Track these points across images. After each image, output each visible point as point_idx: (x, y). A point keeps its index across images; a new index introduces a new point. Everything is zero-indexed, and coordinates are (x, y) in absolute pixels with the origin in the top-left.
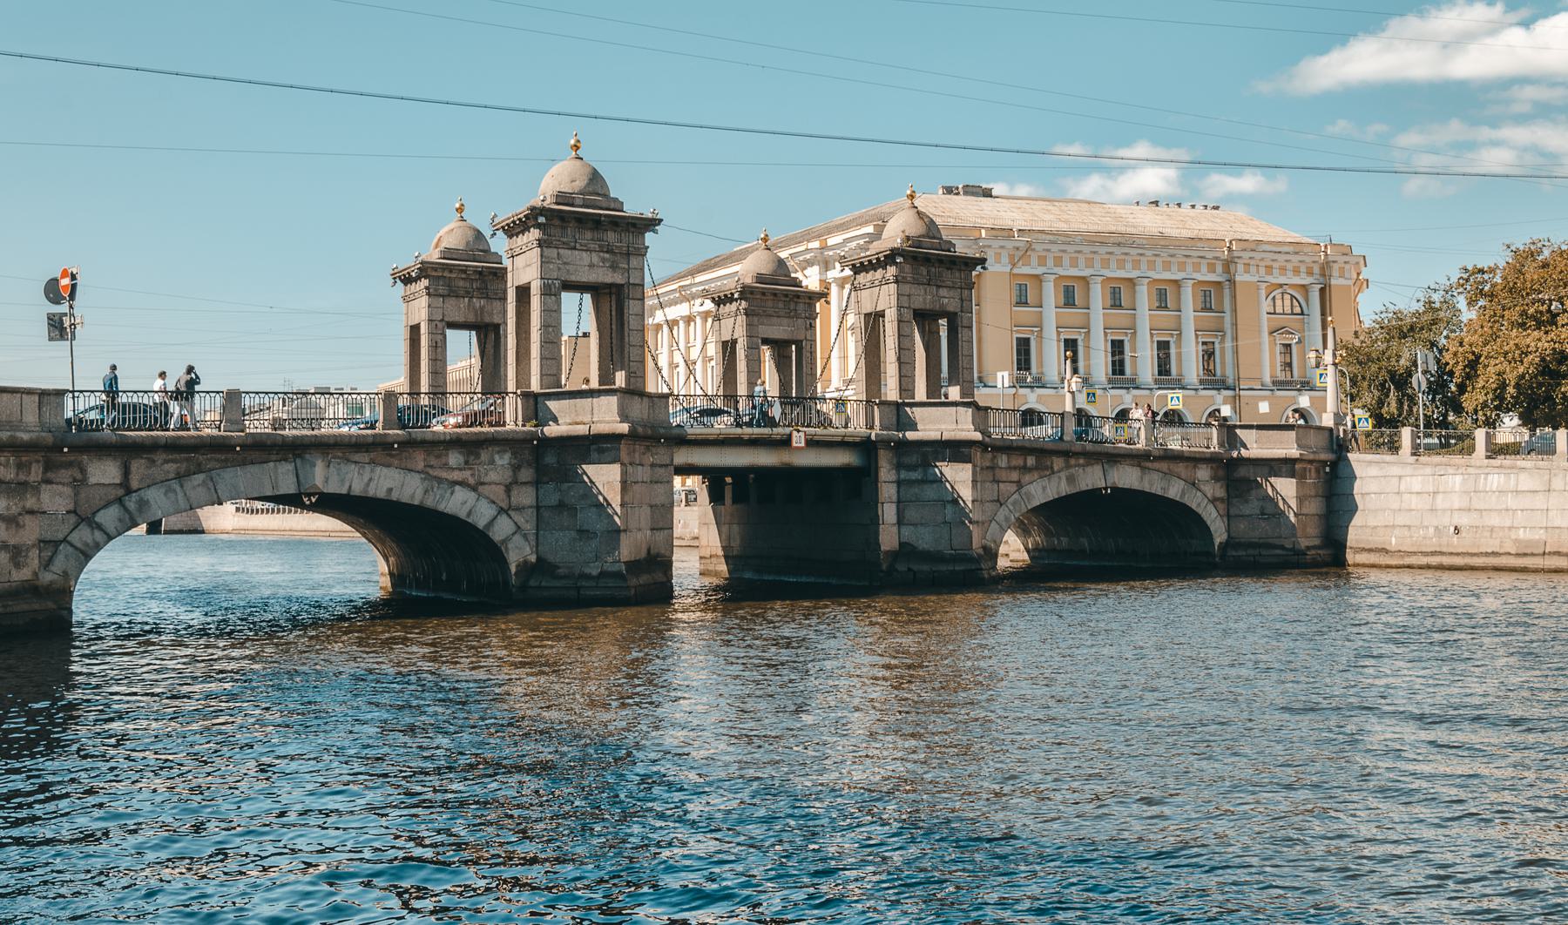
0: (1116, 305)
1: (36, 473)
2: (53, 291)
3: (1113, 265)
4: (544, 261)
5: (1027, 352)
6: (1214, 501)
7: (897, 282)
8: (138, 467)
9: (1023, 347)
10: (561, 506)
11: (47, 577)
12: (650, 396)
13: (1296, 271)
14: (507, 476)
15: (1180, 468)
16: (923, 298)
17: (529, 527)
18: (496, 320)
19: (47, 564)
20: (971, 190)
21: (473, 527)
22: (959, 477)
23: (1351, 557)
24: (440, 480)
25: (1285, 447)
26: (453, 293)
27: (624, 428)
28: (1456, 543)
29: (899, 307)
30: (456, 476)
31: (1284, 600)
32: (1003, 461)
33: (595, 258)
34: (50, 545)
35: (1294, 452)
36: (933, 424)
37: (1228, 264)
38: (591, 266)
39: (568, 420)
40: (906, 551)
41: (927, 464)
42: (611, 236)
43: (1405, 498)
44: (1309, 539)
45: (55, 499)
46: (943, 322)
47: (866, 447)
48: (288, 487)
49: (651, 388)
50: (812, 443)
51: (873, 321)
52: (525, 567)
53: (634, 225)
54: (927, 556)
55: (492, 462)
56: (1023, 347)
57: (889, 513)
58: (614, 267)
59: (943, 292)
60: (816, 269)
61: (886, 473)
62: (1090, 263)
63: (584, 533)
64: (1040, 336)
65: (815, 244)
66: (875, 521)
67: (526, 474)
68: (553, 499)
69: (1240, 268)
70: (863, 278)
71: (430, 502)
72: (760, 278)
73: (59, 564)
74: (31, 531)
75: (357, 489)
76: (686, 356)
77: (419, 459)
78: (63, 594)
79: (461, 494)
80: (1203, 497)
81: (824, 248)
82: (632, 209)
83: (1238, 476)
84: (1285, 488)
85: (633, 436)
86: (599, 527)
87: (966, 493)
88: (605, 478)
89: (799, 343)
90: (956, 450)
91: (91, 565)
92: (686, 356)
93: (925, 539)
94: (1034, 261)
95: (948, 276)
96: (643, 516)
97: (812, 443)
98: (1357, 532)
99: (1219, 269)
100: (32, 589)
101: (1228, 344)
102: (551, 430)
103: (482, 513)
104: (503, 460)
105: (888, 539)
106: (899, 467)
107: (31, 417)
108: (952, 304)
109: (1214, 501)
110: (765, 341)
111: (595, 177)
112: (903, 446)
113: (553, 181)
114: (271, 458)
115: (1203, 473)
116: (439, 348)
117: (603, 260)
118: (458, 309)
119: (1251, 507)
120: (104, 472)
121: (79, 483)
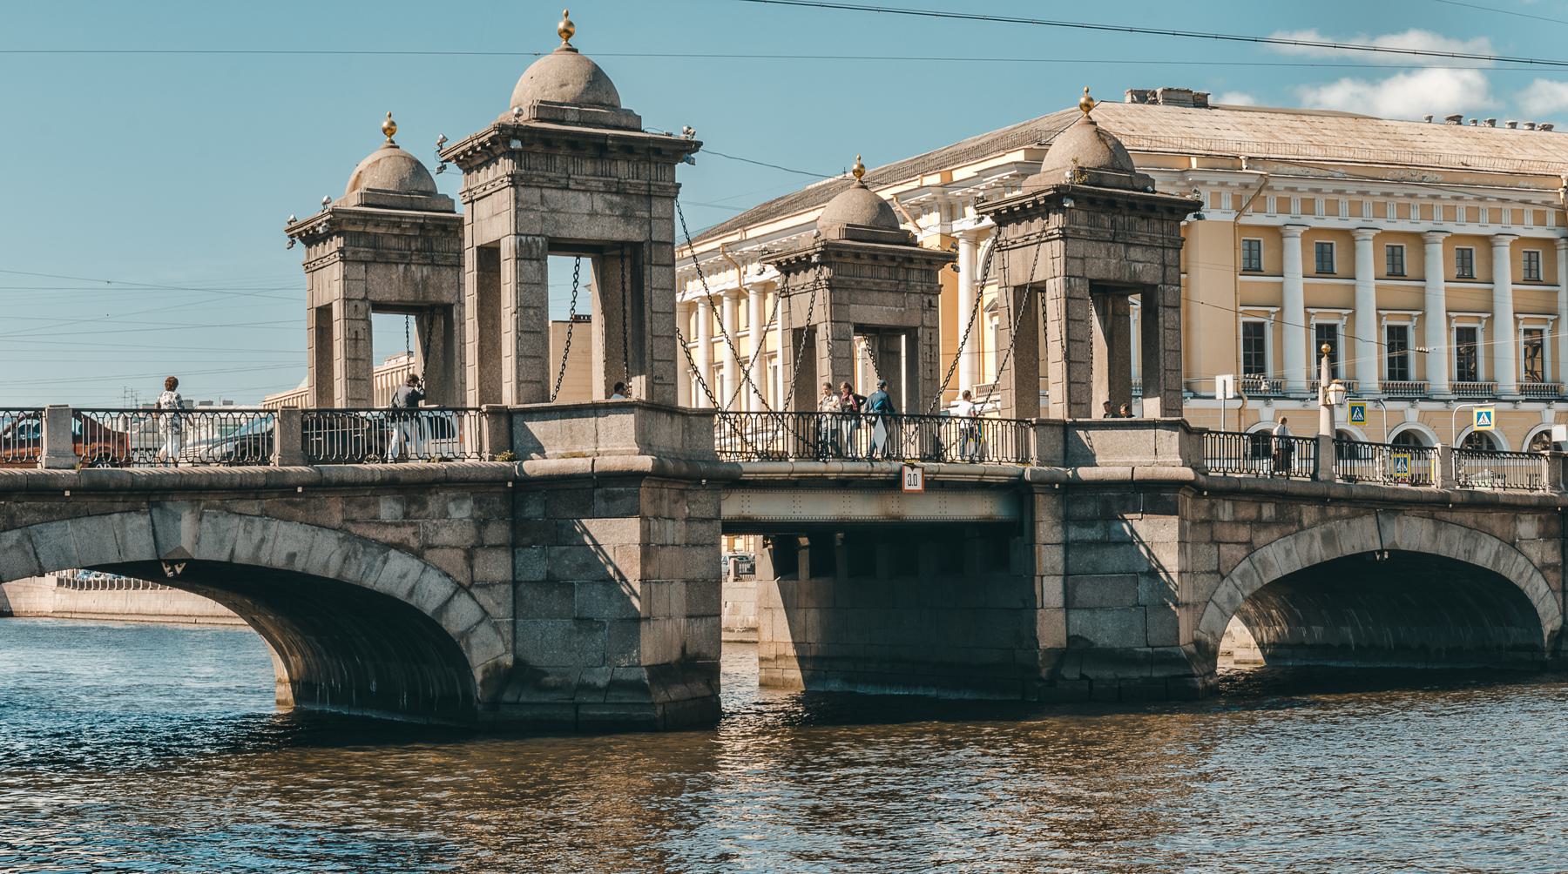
0: (1396, 272)
4: (520, 208)
5: (1260, 345)
6: (1543, 569)
7: (1064, 237)
9: (1254, 337)
10: (551, 581)
12: (685, 414)
14: (468, 535)
16: (1105, 263)
17: (502, 612)
18: (447, 297)
21: (416, 613)
22: (1159, 537)
24: (366, 542)
26: (380, 257)
27: (646, 463)
29: (1068, 277)
30: (391, 535)
32: (1226, 511)
33: (599, 203)
36: (1118, 456)
38: (593, 214)
39: (560, 450)
41: (1110, 516)
42: (622, 169)
46: (1135, 301)
47: (1017, 491)
48: (140, 548)
49: (682, 403)
50: (934, 485)
51: (1028, 297)
52: (497, 674)
53: (658, 152)
55: (445, 514)
57: (1051, 591)
58: (627, 216)
59: (1136, 253)
61: (1047, 530)
62: (1427, 212)
63: (586, 623)
65: (935, 179)
66: (1029, 604)
67: (497, 532)
68: (536, 568)
70: (1011, 232)
71: (351, 575)
72: (851, 231)
75: (243, 555)
76: (738, 351)
81: (947, 185)
82: (654, 126)
86: (608, 612)
87: (1170, 560)
88: (617, 538)
89: (912, 333)
90: (1154, 495)
92: (738, 351)
93: (1106, 631)
95: (1144, 229)
102: (535, 466)
103: (432, 592)
104: (462, 511)
105: (1051, 630)
106: (1067, 521)
108: (1145, 266)
109: (1543, 569)
110: (861, 329)
111: (597, 78)
112: (1074, 489)
113: (534, 84)
115: (1527, 528)
116: (360, 342)
117: (612, 206)
118: (388, 282)
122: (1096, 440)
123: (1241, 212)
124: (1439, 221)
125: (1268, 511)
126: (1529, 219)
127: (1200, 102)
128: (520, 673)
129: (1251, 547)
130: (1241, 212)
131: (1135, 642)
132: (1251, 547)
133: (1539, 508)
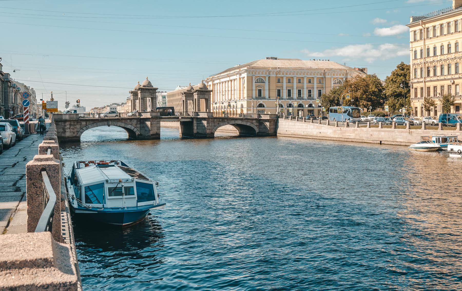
0: (299, 82)
1: (76, 123)
2: (77, 102)
3: (299, 74)
6: (256, 126)
8: (88, 122)
9: (279, 91)
10: (143, 127)
11: (77, 135)
13: (340, 75)
14: (136, 123)
15: (250, 121)
17: (139, 130)
19: (77, 134)
20: (272, 58)
22: (205, 123)
23: (278, 135)
25: (268, 117)
28: (287, 133)
31: (266, 141)
32: (216, 120)
34: (78, 132)
35: (269, 118)
37: (324, 74)
40: (198, 133)
41: (201, 121)
42: (151, 91)
43: (286, 126)
44: (272, 131)
45: (78, 126)
47: (192, 118)
50: (182, 118)
52: (138, 135)
54: (201, 134)
56: (279, 91)
57: (195, 128)
60: (238, 75)
61: (195, 122)
63: (146, 130)
64: (293, 89)
65: (238, 70)
66: (193, 129)
67: (138, 123)
68: (142, 126)
69: (327, 74)
72: (188, 91)
73: (79, 134)
74: (75, 130)
77: (124, 121)
78: (79, 137)
79: (129, 125)
80: (254, 126)
81: (240, 71)
83: (260, 122)
84: (268, 124)
85: (152, 118)
86: (148, 130)
87: (206, 125)
88: (148, 123)
90: (204, 119)
91: (82, 135)
93: (200, 131)
94: (281, 74)
96: (155, 128)
97: (182, 118)
98: (278, 131)
99: (322, 75)
100: (76, 137)
101: (324, 90)
102: (142, 117)
104: (135, 121)
105: (195, 131)
106: (197, 121)
107: (75, 117)
109: (256, 126)
111: (149, 82)
112: (197, 118)
113: (143, 83)
114: (112, 120)
115: (254, 121)
119: (262, 127)
120: (84, 123)
121: (81, 124)
122: (200, 114)
123: (277, 75)
124: (305, 75)
125: (221, 120)
126: (319, 75)
127: (276, 59)
128: (141, 135)
129: (218, 124)
130: (277, 75)
131: (203, 132)
132: (218, 124)
133: (256, 119)
